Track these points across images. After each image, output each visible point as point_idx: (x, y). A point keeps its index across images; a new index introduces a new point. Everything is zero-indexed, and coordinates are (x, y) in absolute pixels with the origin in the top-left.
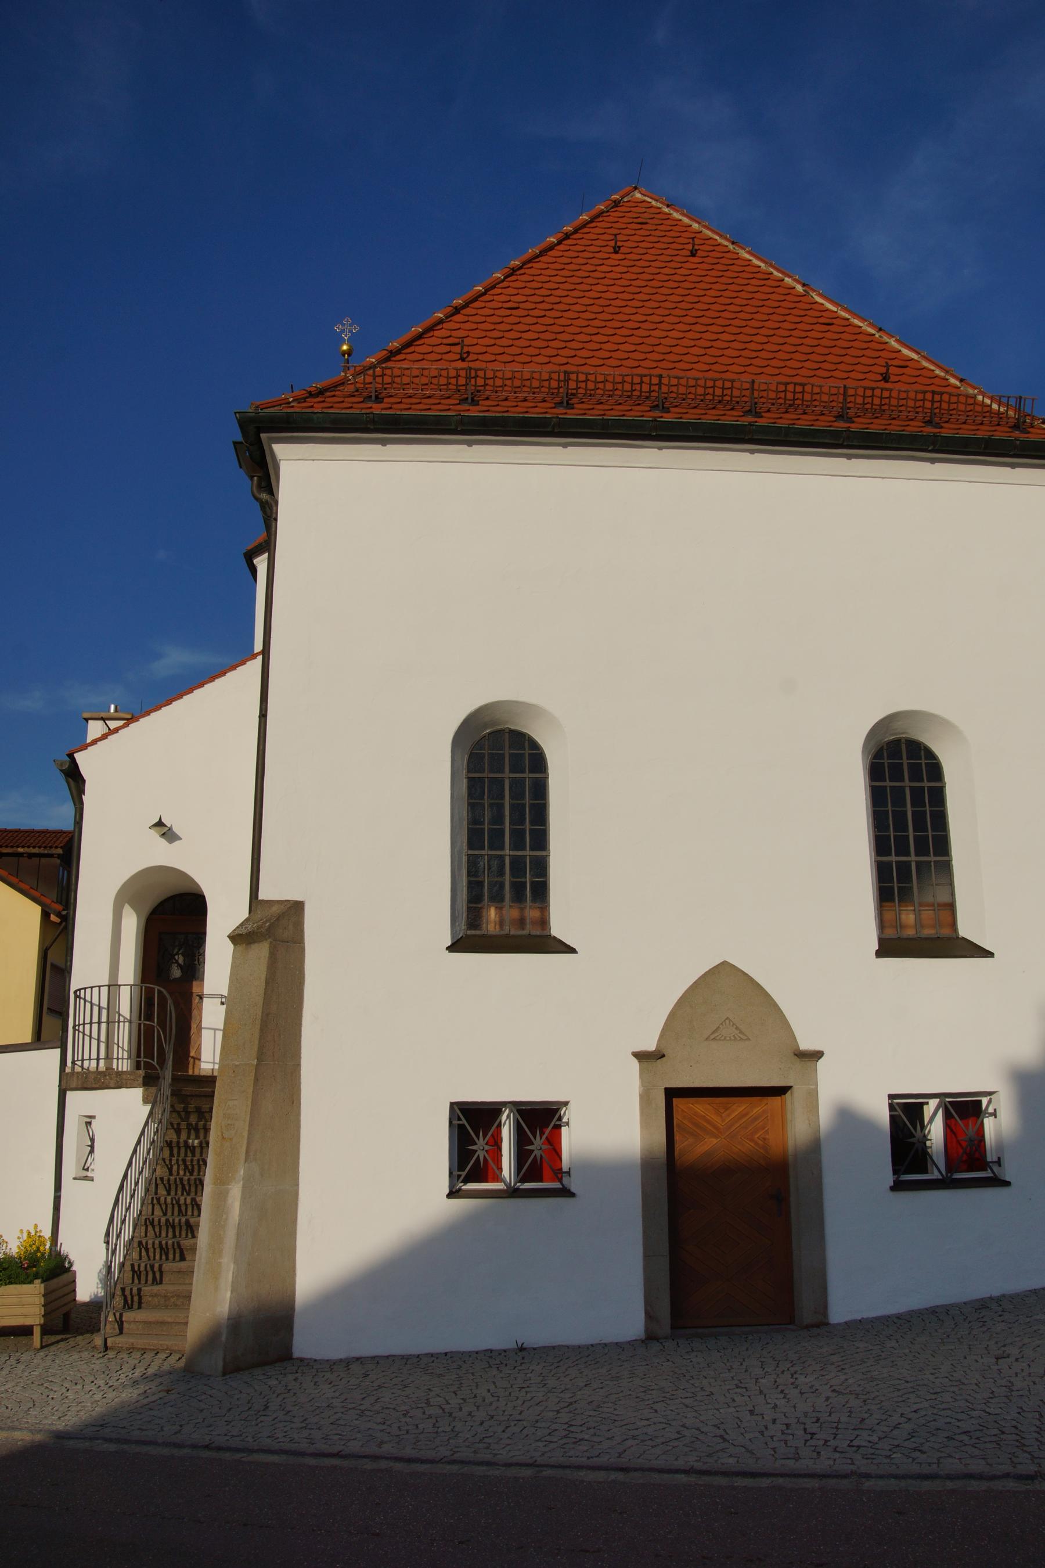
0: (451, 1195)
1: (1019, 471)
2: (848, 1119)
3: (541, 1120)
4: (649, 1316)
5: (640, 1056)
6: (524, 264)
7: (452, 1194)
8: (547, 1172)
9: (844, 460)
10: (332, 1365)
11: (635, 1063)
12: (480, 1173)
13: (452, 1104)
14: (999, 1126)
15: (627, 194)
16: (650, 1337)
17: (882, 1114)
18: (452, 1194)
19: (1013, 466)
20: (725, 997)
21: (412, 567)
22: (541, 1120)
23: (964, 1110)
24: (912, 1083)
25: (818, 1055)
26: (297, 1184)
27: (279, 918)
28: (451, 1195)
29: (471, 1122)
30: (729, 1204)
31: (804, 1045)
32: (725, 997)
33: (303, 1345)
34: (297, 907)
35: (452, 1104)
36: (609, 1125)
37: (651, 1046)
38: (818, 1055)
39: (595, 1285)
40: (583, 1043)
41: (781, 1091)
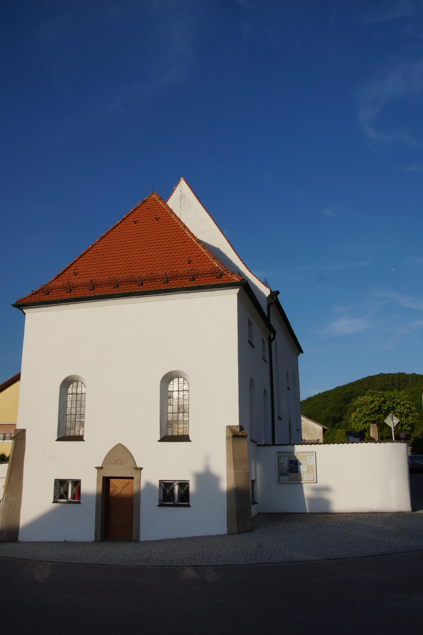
0: (54, 502)
1: (215, 292)
2: (149, 485)
3: (77, 483)
4: (96, 536)
5: (98, 468)
6: (106, 234)
7: (54, 502)
8: (76, 497)
9: (163, 296)
10: (24, 542)
11: (96, 470)
12: (61, 497)
13: (56, 480)
14: (192, 488)
15: (149, 197)
16: (96, 541)
17: (157, 484)
18: (54, 502)
19: (213, 291)
20: (120, 453)
21: (56, 337)
22: (77, 483)
23: (184, 485)
24: (168, 477)
25: (141, 469)
26: (21, 498)
27: (19, 433)
28: (54, 502)
29: (61, 484)
30: (116, 508)
31: (138, 466)
32: (120, 453)
33: (21, 538)
34: (24, 431)
35: (56, 480)
36: (90, 486)
37: (100, 465)
38: (141, 469)
39: (83, 526)
40: (84, 466)
41: (132, 478)
